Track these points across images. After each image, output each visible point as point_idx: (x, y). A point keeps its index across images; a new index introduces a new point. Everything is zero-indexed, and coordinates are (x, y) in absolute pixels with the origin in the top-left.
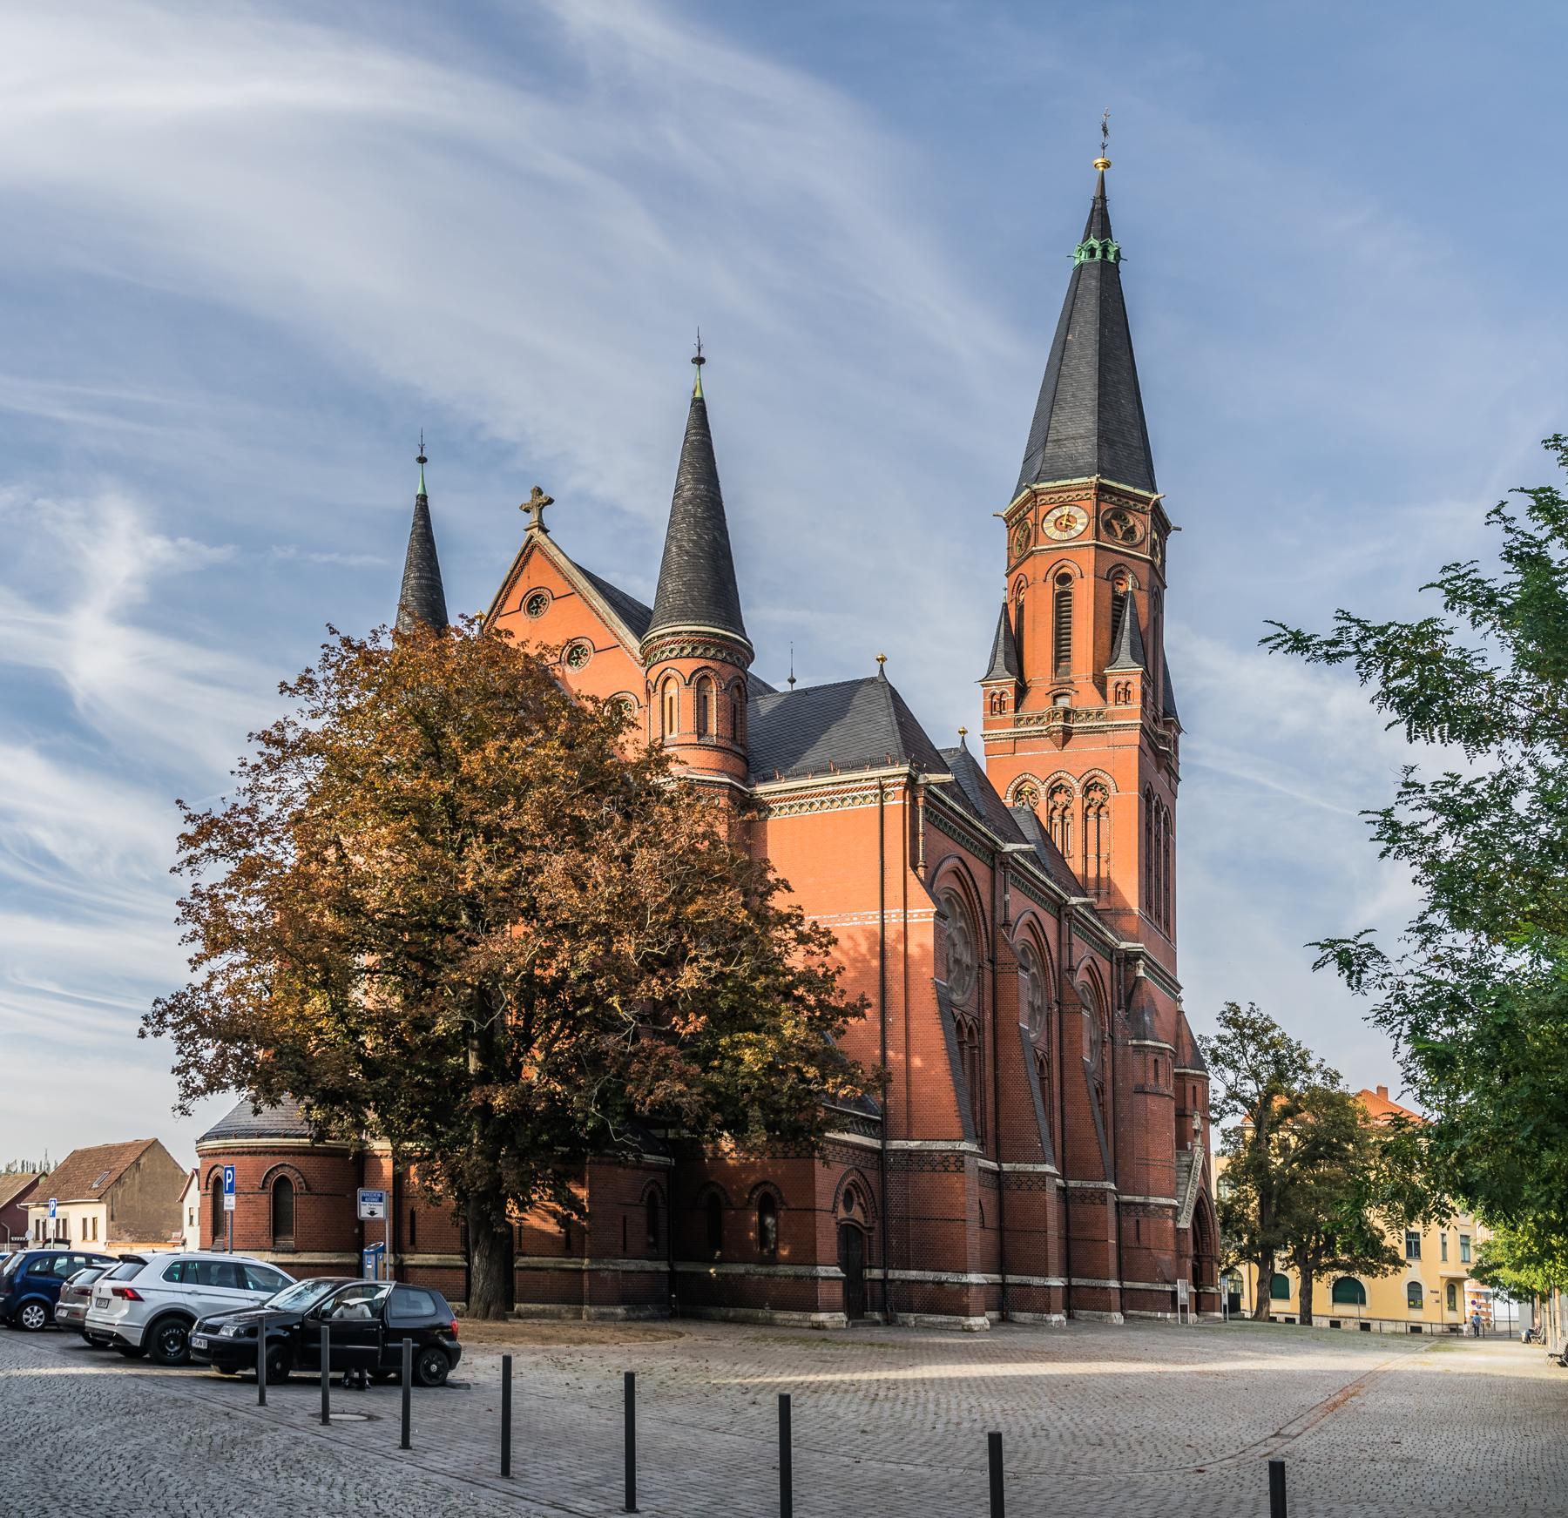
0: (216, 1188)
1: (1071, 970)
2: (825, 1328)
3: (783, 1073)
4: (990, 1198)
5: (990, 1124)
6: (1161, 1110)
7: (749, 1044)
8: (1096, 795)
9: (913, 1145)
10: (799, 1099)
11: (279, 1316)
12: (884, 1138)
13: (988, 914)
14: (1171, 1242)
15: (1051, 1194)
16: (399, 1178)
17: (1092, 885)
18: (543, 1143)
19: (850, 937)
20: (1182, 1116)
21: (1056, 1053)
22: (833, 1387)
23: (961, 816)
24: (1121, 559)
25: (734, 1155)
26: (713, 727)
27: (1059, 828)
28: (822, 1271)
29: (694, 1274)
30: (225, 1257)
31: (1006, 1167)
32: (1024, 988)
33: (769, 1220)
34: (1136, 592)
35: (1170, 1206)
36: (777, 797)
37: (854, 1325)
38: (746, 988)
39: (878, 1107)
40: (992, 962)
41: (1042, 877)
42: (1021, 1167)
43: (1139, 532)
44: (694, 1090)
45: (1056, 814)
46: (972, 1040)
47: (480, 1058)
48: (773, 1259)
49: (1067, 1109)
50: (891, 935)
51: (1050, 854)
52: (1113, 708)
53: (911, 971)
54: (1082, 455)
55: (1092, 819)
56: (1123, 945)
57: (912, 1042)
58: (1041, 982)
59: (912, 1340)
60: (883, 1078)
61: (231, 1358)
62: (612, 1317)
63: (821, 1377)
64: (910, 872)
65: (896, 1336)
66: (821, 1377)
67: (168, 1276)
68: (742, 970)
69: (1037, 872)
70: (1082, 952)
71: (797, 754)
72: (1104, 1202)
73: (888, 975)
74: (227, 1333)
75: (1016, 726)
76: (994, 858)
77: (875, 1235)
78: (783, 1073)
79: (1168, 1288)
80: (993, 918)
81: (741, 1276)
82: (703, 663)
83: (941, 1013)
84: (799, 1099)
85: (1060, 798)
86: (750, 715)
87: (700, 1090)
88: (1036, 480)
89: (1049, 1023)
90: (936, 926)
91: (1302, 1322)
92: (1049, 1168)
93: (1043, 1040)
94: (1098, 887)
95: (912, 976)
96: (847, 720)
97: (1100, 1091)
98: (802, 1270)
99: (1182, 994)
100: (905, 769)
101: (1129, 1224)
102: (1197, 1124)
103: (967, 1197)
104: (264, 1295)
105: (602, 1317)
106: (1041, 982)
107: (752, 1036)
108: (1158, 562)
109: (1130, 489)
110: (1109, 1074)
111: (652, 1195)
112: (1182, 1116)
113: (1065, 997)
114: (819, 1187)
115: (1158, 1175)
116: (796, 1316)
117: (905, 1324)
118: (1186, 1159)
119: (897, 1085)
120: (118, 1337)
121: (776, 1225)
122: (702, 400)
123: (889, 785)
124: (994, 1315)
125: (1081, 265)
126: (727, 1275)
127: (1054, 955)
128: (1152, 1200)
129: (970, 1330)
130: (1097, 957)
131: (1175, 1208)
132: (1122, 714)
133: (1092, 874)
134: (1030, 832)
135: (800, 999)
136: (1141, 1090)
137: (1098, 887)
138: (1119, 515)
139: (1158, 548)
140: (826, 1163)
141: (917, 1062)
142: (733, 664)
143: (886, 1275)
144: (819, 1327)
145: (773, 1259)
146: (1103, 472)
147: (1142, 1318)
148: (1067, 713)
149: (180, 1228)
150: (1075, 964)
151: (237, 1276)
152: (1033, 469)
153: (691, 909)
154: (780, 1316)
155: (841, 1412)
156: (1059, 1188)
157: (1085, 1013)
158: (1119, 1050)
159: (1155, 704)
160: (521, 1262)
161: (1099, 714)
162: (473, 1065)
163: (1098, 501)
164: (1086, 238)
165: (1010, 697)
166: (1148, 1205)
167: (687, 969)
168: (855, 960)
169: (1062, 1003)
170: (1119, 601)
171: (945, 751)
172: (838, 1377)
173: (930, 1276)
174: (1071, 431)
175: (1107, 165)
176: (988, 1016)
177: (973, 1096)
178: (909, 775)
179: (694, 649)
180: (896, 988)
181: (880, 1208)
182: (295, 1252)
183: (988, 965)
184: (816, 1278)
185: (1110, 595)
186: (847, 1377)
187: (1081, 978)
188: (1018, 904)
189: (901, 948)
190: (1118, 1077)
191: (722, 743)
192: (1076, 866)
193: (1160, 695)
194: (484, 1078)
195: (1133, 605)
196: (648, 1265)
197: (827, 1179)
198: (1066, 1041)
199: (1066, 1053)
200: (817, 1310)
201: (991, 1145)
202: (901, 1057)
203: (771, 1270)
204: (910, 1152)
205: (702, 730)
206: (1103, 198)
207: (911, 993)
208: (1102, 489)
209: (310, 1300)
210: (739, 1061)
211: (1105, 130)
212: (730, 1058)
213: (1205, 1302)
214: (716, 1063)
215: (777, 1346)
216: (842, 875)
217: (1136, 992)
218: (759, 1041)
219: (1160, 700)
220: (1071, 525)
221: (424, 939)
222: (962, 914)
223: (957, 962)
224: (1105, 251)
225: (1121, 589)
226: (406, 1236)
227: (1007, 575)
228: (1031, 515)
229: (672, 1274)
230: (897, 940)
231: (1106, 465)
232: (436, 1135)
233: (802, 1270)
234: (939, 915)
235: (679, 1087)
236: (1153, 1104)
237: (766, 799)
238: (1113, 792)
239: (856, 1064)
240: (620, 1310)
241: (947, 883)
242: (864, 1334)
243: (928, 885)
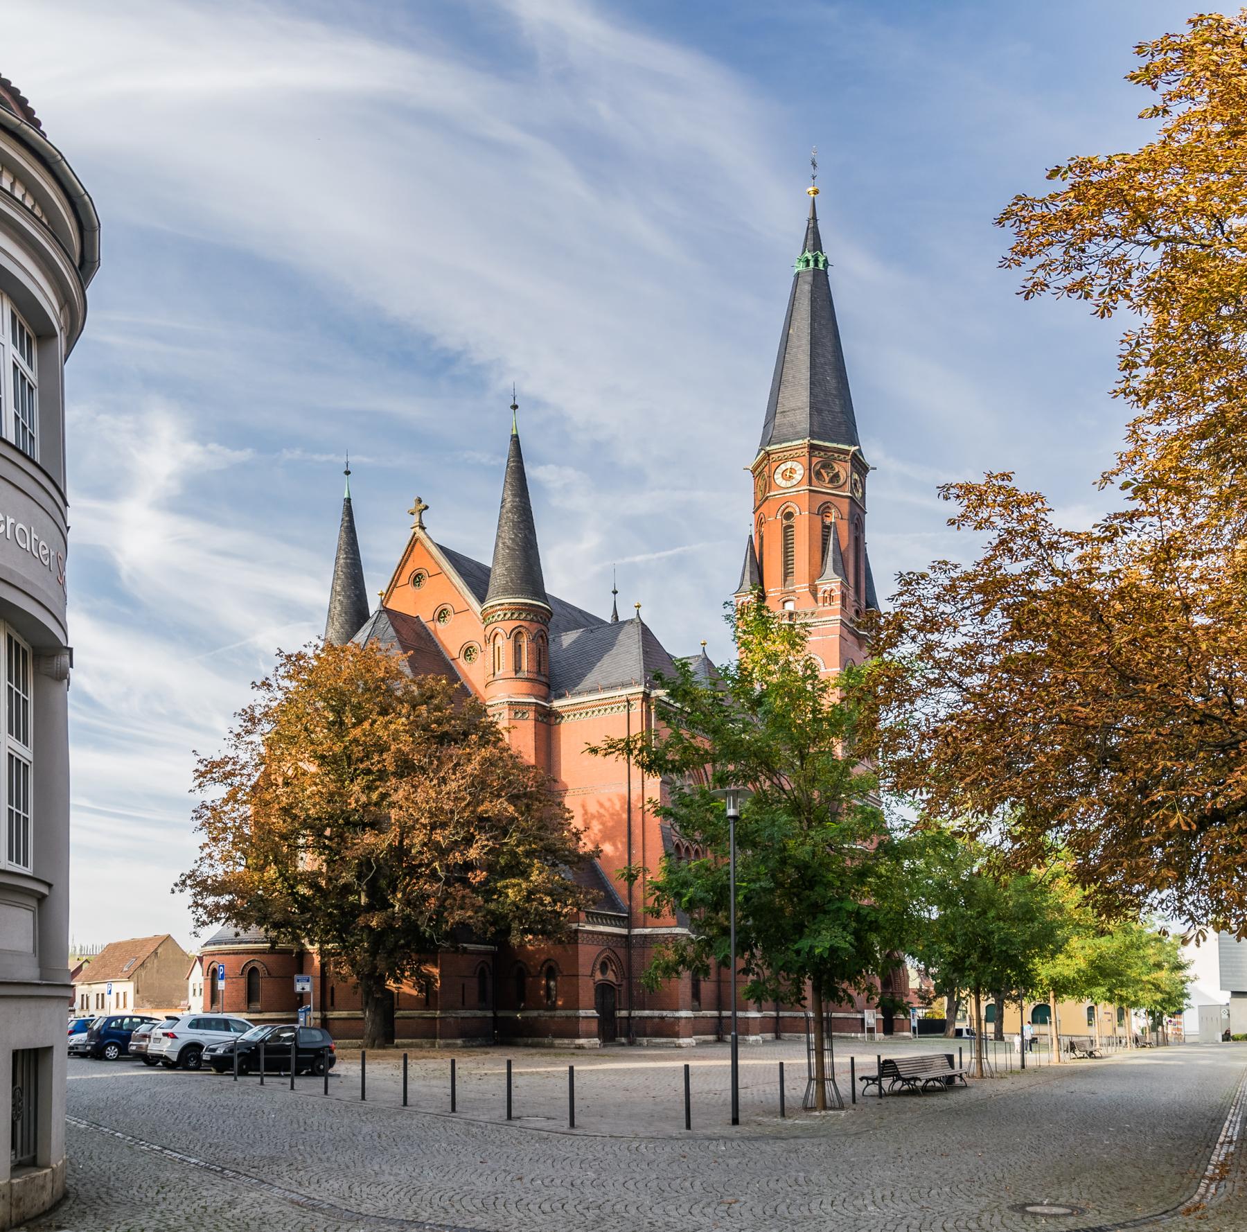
0: (213, 975)
9: (647, 931)
11: (247, 1044)
12: (630, 927)
16: (323, 965)
18: (408, 942)
19: (610, 800)
24: (828, 498)
26: (525, 666)
28: (582, 1013)
29: (508, 1018)
30: (219, 1016)
33: (552, 983)
34: (839, 521)
39: (626, 908)
43: (843, 475)
47: (367, 896)
48: (554, 1007)
54: (800, 422)
61: (221, 1064)
62: (454, 1046)
67: (191, 1026)
71: (581, 677)
74: (220, 1052)
77: (623, 989)
79: (859, 1016)
82: (518, 623)
88: (769, 444)
91: (996, 1039)
95: (647, 824)
96: (613, 652)
98: (570, 1013)
100: (642, 689)
104: (238, 1034)
105: (447, 1046)
108: (858, 495)
109: (835, 445)
111: (482, 971)
114: (581, 960)
116: (566, 1041)
117: (641, 1045)
120: (166, 1057)
122: (517, 436)
124: (769, 1036)
125: (798, 274)
129: (680, 1047)
138: (827, 465)
139: (859, 484)
142: (538, 622)
144: (580, 1047)
145: (554, 1007)
146: (813, 435)
148: (791, 615)
149: (186, 997)
151: (225, 1025)
154: (558, 1041)
159: (857, 601)
160: (398, 1014)
161: (813, 614)
162: (364, 900)
163: (810, 457)
164: (804, 251)
168: (612, 815)
170: (826, 528)
173: (656, 1013)
174: (793, 405)
175: (816, 192)
182: (260, 1012)
185: (820, 525)
191: (531, 676)
194: (370, 908)
195: (836, 532)
196: (479, 1013)
197: (587, 954)
200: (579, 1037)
203: (552, 1013)
204: (645, 936)
205: (517, 669)
206: (814, 218)
208: (813, 447)
209: (262, 1034)
211: (814, 164)
220: (792, 476)
221: (333, 830)
224: (816, 261)
225: (828, 521)
226: (329, 1001)
228: (767, 469)
229: (495, 1018)
230: (637, 801)
231: (816, 429)
232: (343, 941)
233: (570, 1013)
240: (459, 1042)
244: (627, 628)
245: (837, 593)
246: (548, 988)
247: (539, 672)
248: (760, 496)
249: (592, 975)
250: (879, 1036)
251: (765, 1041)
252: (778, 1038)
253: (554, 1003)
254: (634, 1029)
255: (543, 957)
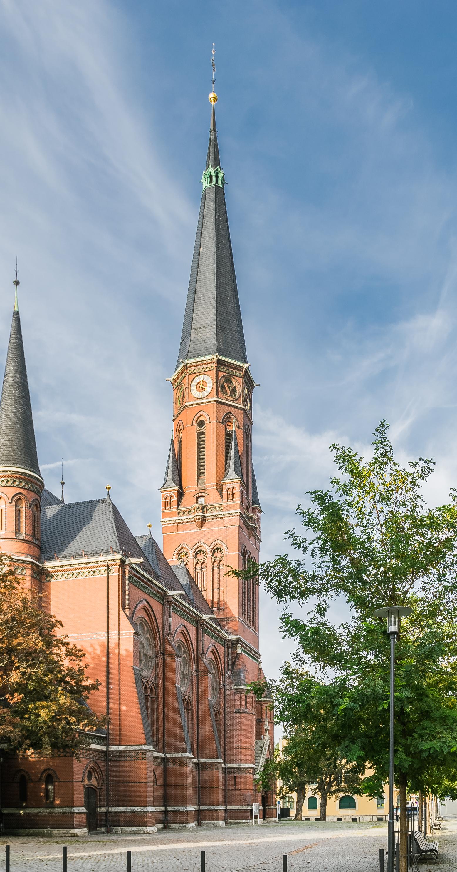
1: (203, 653)
2: (77, 836)
3: (60, 720)
4: (160, 771)
5: (159, 737)
6: (248, 721)
7: (43, 707)
8: (218, 555)
9: (122, 748)
10: (66, 732)
12: (108, 745)
13: (161, 629)
14: (251, 786)
15: (190, 766)
17: (216, 605)
19: (92, 646)
20: (259, 722)
21: (195, 697)
22: (81, 858)
23: (148, 579)
25: (33, 756)
26: (23, 529)
27: (199, 574)
28: (76, 810)
31: (168, 755)
32: (178, 666)
33: (50, 787)
35: (251, 768)
36: (56, 569)
37: (91, 834)
38: (42, 680)
40: (163, 654)
41: (189, 606)
42: (175, 755)
44: (17, 730)
45: (198, 566)
46: (152, 695)
48: (52, 805)
49: (200, 724)
50: (112, 644)
51: (193, 589)
52: (226, 504)
53: (122, 662)
55: (216, 568)
56: (231, 637)
57: (122, 698)
58: (188, 661)
59: (119, 839)
60: (107, 721)
63: (76, 855)
64: (121, 611)
65: (112, 837)
66: (76, 855)
68: (39, 671)
69: (186, 604)
70: (209, 643)
71: (65, 544)
72: (217, 769)
73: (110, 665)
75: (178, 516)
76: (165, 599)
78: (60, 720)
80: (163, 631)
81: (37, 814)
82: (18, 490)
83: (136, 683)
84: (66, 732)
85: (200, 557)
86: (42, 518)
87: (20, 729)
88: (186, 358)
89: (192, 682)
90: (134, 639)
92: (189, 755)
93: (188, 690)
94: (219, 606)
96: (91, 525)
97: (217, 714)
98: (66, 810)
99: (261, 659)
100: (119, 556)
101: (231, 778)
102: (266, 726)
103: (147, 772)
106: (188, 661)
107: (44, 703)
110: (222, 704)
112: (259, 722)
113: (200, 668)
114: (75, 770)
115: (246, 753)
116: (63, 831)
118: (260, 744)
119: (114, 719)
121: (54, 789)
123: (112, 565)
124: (160, 826)
126: (29, 814)
127: (195, 646)
128: (242, 766)
129: (147, 833)
130: (217, 645)
131: (254, 769)
132: (230, 507)
133: (216, 599)
134: (183, 580)
135: (68, 682)
136: (238, 712)
137: (219, 606)
138: (228, 380)
140: (79, 760)
141: (124, 708)
142: (34, 492)
143: (107, 810)
144: (75, 835)
145: (52, 805)
147: (236, 823)
148: (203, 507)
150: (205, 651)
152: (185, 348)
153: (15, 642)
154: (55, 832)
155: (84, 866)
156: (194, 763)
157: (210, 676)
158: (228, 692)
159: (247, 499)
161: (219, 508)
163: (218, 371)
165: (175, 499)
166: (240, 768)
167: (14, 672)
168: (94, 657)
169: (198, 670)
170: (229, 436)
171: (138, 537)
172: (83, 854)
173: (129, 809)
176: (160, 681)
177: (152, 722)
178: (121, 559)
179: (14, 481)
180: (114, 671)
181: (105, 778)
183: (160, 656)
184: (73, 813)
186: (87, 854)
187: (209, 656)
188: (176, 622)
189: (117, 651)
190: (227, 706)
191: (28, 538)
192: (207, 595)
193: (250, 492)
198: (200, 690)
199: (200, 696)
200: (73, 828)
201: (161, 745)
202: (116, 706)
204: (120, 752)
205: (17, 531)
207: (121, 673)
210: (38, 715)
212: (34, 713)
213: (268, 813)
214: (27, 716)
215: (54, 844)
216: (88, 614)
217: (237, 662)
218: (48, 706)
219: (251, 495)
220: (204, 387)
222: (148, 630)
223: (145, 655)
225: (229, 429)
227: (174, 421)
228: (184, 381)
230: (115, 647)
233: (66, 810)
234: (136, 634)
235: (10, 728)
236: (244, 718)
237: (50, 570)
238: (226, 553)
239: (93, 715)
241: (140, 615)
242: (96, 838)
243: (130, 618)
244: (100, 506)
245: (237, 491)
246: (47, 791)
247: (34, 536)
248: (178, 406)
249: (82, 781)
250: (261, 821)
251: (159, 830)
252: (199, 825)
253: (53, 801)
254: (110, 821)
255: (43, 767)
